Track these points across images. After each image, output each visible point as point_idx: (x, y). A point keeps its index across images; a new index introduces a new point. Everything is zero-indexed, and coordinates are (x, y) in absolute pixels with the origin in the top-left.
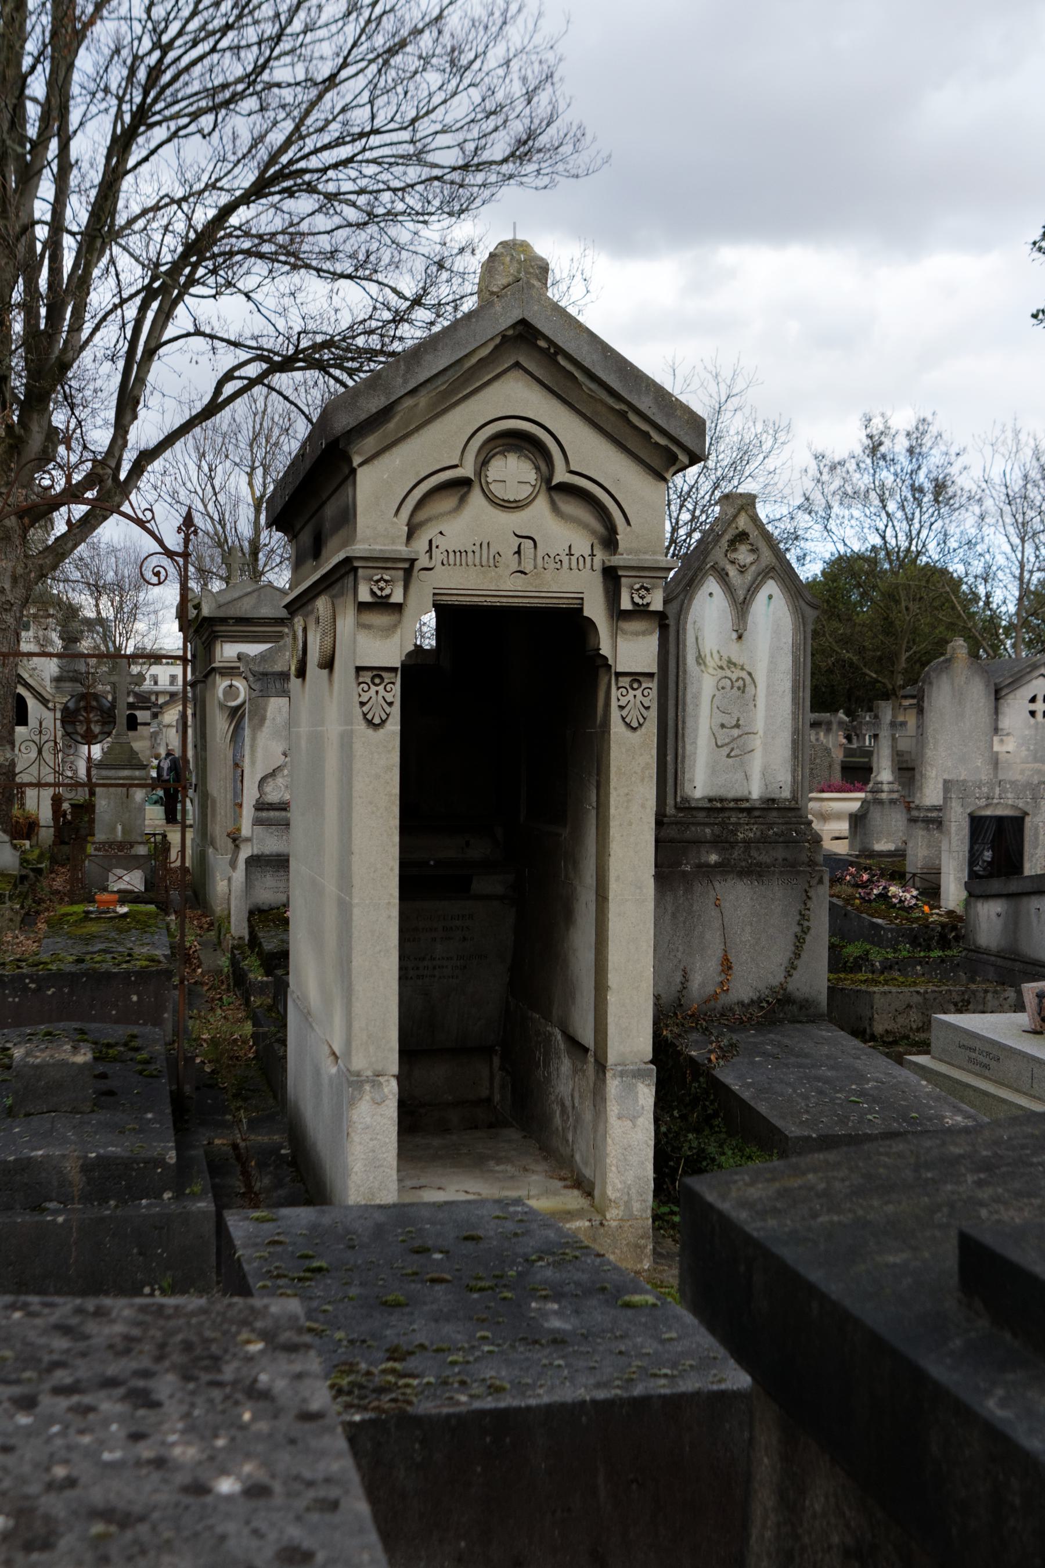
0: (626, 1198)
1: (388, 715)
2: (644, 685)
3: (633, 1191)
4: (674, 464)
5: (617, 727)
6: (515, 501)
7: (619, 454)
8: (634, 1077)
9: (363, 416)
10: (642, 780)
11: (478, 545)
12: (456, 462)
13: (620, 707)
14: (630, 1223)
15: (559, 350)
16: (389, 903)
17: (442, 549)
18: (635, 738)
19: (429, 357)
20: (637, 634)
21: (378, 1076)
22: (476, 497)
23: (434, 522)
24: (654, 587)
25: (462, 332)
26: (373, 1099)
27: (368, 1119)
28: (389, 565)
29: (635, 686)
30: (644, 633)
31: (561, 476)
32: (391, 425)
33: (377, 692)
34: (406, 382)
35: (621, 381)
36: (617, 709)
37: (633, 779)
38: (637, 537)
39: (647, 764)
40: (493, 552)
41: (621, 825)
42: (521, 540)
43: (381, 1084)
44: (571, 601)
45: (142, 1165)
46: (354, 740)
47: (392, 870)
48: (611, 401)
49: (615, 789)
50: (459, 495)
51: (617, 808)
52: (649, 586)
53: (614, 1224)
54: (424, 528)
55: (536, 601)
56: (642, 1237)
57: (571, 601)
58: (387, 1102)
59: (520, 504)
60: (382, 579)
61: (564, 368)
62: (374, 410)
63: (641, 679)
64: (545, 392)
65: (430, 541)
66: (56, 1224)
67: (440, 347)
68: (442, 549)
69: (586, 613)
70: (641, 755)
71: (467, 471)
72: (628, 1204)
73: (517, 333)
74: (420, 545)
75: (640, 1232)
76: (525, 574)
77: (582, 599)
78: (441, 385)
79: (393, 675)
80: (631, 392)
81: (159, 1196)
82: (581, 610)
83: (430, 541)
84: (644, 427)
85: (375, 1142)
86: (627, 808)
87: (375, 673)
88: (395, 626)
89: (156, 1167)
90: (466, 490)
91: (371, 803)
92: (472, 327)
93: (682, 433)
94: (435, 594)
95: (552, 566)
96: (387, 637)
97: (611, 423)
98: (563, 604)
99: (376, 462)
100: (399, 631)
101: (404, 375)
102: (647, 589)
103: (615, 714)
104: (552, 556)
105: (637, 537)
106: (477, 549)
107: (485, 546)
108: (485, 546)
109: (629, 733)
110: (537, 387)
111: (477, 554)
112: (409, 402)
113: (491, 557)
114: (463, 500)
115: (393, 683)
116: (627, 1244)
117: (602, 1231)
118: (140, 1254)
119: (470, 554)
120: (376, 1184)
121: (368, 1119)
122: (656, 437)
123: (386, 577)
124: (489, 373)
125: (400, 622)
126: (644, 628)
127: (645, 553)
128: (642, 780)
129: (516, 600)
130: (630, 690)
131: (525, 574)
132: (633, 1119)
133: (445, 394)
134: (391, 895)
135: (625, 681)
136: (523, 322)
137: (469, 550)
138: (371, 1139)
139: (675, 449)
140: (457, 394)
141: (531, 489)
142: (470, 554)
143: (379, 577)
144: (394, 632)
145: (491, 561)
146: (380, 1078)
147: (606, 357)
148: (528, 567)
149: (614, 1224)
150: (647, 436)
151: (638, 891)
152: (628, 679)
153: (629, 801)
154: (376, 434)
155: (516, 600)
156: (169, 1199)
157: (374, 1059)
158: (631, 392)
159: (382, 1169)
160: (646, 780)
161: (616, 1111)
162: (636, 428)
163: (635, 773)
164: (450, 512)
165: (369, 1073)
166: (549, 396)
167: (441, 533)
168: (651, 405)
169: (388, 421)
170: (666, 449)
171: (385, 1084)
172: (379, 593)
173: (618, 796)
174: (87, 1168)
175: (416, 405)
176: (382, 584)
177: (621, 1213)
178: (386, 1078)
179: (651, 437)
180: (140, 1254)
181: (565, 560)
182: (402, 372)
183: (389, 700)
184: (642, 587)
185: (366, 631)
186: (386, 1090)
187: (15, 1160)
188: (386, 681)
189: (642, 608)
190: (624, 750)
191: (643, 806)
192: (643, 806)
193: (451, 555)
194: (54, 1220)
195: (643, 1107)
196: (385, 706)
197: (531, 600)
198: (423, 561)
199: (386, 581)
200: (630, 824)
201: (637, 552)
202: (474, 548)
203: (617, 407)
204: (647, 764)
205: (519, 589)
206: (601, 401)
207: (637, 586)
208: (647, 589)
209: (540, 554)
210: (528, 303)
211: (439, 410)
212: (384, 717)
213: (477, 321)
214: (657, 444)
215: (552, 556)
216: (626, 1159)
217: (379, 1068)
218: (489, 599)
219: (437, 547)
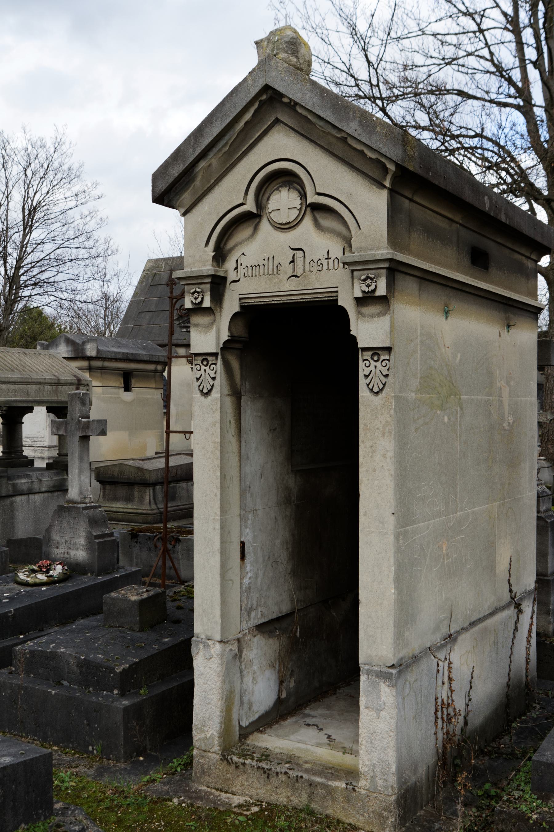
0: (371, 774)
1: (384, 385)
2: (382, 358)
3: (377, 770)
4: (387, 173)
5: (364, 393)
6: (287, 224)
7: (351, 173)
8: (377, 676)
9: (171, 180)
10: (383, 435)
11: (266, 259)
12: (241, 201)
13: (365, 375)
14: (375, 795)
15: (296, 104)
16: (214, 519)
17: (244, 266)
18: (377, 400)
19: (207, 130)
20: (373, 316)
21: (209, 640)
22: (265, 225)
23: (239, 247)
24: (378, 276)
25: (228, 106)
26: (205, 655)
27: (202, 668)
28: (200, 281)
29: (376, 358)
30: (379, 315)
31: (312, 198)
32: (198, 182)
33: (205, 370)
34: (194, 150)
35: (334, 114)
36: (363, 377)
37: (376, 434)
38: (365, 237)
39: (387, 422)
40: (276, 263)
41: (367, 471)
42: (295, 252)
43: (208, 645)
44: (330, 295)
45: (104, 669)
46: (194, 404)
47: (216, 495)
48: (334, 132)
49: (363, 441)
50: (254, 225)
51: (364, 457)
52: (373, 276)
53: (363, 792)
54: (233, 252)
55: (306, 297)
56: (385, 810)
57: (330, 295)
58: (213, 659)
59: (292, 225)
60: (195, 292)
61: (301, 114)
62: (177, 175)
63: (380, 352)
64: (298, 137)
65: (237, 261)
66: (51, 694)
67: (214, 121)
68: (244, 266)
69: (340, 303)
70: (382, 414)
71: (250, 206)
72: (373, 778)
73: (269, 96)
74: (230, 265)
75: (383, 805)
76: (298, 277)
77: (337, 292)
78: (224, 146)
79: (214, 358)
80: (341, 121)
81: (112, 692)
82: (337, 300)
83: (237, 261)
84: (359, 147)
85: (207, 685)
86: (372, 457)
87: (204, 357)
88: (212, 324)
89: (110, 673)
90: (258, 220)
91: (203, 448)
92: (234, 100)
93: (381, 145)
94: (240, 299)
95: (315, 268)
96: (208, 331)
97: (339, 149)
98: (325, 297)
99: (194, 210)
100: (215, 327)
101: (193, 146)
102: (371, 279)
103: (362, 382)
104: (316, 261)
105: (365, 237)
106: (266, 262)
107: (271, 259)
108: (271, 259)
109: (373, 397)
110: (292, 134)
111: (266, 266)
112: (202, 164)
113: (275, 267)
114: (256, 228)
115: (215, 364)
116: (373, 812)
117: (354, 795)
118: (88, 725)
119: (262, 267)
120: (207, 716)
121: (202, 668)
122: (370, 154)
123: (198, 290)
124: (258, 131)
125: (215, 320)
126: (378, 311)
127: (371, 249)
128: (383, 435)
129: (293, 298)
130: (372, 362)
131: (298, 277)
132: (378, 711)
133: (230, 153)
134: (216, 513)
135: (368, 355)
136: (267, 88)
137: (261, 264)
138: (204, 683)
139: (383, 160)
140: (239, 151)
141: (298, 212)
142: (262, 267)
143: (193, 290)
144: (212, 328)
145: (275, 270)
146: (209, 642)
147: (323, 98)
148: (299, 272)
149: (363, 792)
150: (362, 152)
151: (381, 525)
152: (370, 353)
153: (373, 452)
154: (188, 191)
155: (293, 298)
156: (116, 694)
157: (206, 627)
158: (341, 121)
159: (210, 705)
160: (386, 434)
161: (364, 702)
162: (355, 149)
163: (378, 429)
164: (249, 238)
165: (203, 637)
166: (301, 139)
167: (243, 254)
168: (358, 128)
169: (193, 180)
170: (378, 161)
171: (212, 646)
172: (194, 301)
173: (365, 447)
174: (82, 664)
175: (210, 165)
176: (196, 295)
177: (368, 785)
178: (213, 642)
179: (366, 155)
180: (88, 725)
181: (325, 262)
182: (192, 144)
183: (384, 374)
184: (368, 278)
185: (196, 328)
186: (212, 651)
187: (50, 652)
188: (210, 362)
189: (369, 295)
190: (369, 411)
191: (384, 456)
192: (384, 456)
193: (250, 268)
194: (50, 692)
195: (384, 704)
196: (210, 380)
197: (303, 297)
198: (232, 276)
199: (198, 293)
200: (374, 470)
201: (366, 249)
202: (265, 262)
203: (339, 136)
204: (387, 422)
205: (294, 289)
206: (329, 133)
207: (363, 277)
208: (371, 279)
209: (307, 261)
210: (269, 71)
211: (228, 165)
212: (381, 386)
213: (236, 95)
214: (371, 158)
215: (316, 261)
216: (372, 743)
217: (209, 634)
218: (275, 299)
219: (241, 264)
